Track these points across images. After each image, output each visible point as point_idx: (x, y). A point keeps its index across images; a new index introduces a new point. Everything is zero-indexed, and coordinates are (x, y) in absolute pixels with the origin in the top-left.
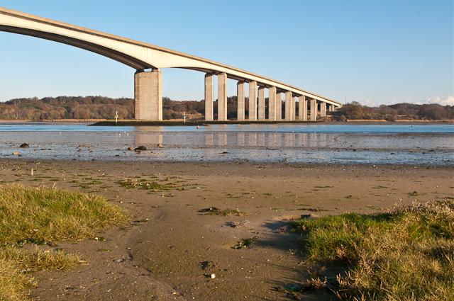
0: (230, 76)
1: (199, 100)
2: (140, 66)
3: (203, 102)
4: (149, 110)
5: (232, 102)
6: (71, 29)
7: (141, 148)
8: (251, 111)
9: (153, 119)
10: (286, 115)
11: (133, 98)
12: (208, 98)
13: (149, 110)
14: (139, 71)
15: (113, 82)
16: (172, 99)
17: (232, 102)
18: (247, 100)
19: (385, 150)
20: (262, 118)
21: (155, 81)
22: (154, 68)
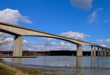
0: (96, 46)
1: (90, 51)
2: (17, 36)
3: (91, 52)
4: (17, 53)
5: (97, 52)
6: (38, 32)
7: (102, 59)
8: (101, 54)
9: (18, 56)
10: (108, 55)
11: (76, 51)
12: (92, 50)
13: (17, 53)
14: (15, 39)
15: (73, 48)
16: (84, 51)
17: (97, 52)
18: (93, 52)
19: (105, 69)
20: (103, 55)
21: (81, 48)
22: (81, 45)
